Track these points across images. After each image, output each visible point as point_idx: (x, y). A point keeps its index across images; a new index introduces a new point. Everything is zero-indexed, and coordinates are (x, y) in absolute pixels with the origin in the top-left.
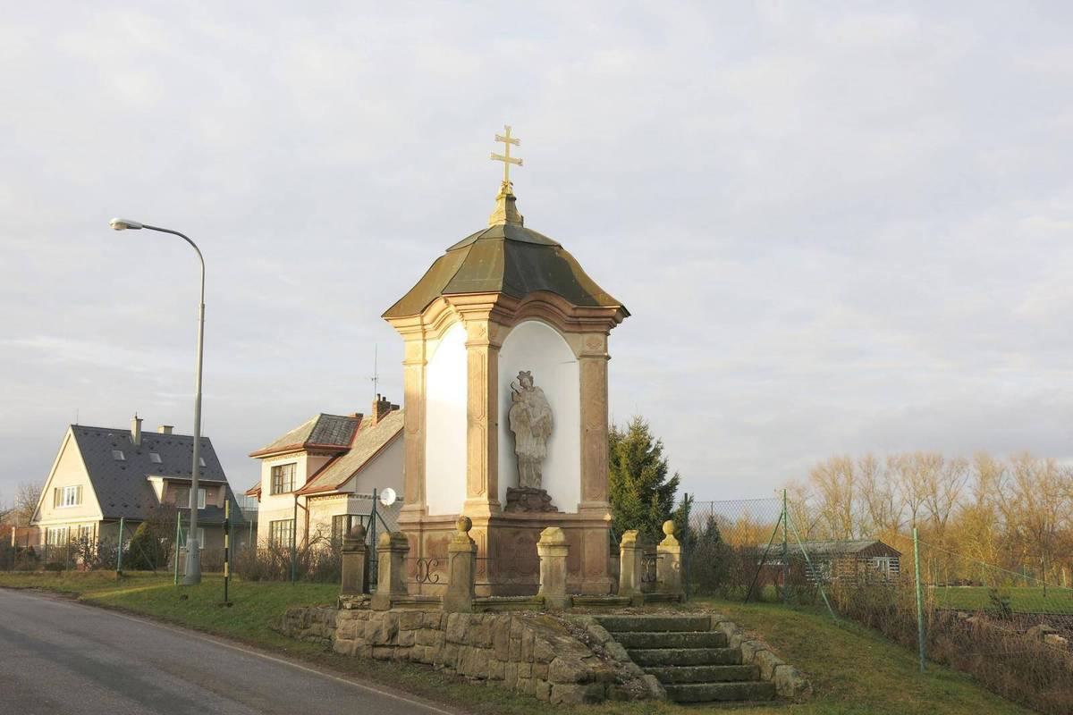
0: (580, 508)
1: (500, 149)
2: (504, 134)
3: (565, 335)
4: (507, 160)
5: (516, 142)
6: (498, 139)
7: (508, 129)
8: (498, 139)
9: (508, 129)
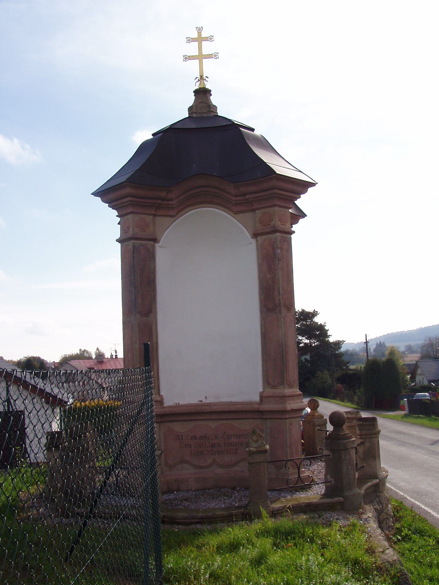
0: (262, 397)
1: (193, 49)
2: (195, 35)
3: (237, 216)
4: (201, 57)
5: (210, 39)
6: (190, 40)
7: (199, 30)
8: (190, 40)
9: (199, 30)
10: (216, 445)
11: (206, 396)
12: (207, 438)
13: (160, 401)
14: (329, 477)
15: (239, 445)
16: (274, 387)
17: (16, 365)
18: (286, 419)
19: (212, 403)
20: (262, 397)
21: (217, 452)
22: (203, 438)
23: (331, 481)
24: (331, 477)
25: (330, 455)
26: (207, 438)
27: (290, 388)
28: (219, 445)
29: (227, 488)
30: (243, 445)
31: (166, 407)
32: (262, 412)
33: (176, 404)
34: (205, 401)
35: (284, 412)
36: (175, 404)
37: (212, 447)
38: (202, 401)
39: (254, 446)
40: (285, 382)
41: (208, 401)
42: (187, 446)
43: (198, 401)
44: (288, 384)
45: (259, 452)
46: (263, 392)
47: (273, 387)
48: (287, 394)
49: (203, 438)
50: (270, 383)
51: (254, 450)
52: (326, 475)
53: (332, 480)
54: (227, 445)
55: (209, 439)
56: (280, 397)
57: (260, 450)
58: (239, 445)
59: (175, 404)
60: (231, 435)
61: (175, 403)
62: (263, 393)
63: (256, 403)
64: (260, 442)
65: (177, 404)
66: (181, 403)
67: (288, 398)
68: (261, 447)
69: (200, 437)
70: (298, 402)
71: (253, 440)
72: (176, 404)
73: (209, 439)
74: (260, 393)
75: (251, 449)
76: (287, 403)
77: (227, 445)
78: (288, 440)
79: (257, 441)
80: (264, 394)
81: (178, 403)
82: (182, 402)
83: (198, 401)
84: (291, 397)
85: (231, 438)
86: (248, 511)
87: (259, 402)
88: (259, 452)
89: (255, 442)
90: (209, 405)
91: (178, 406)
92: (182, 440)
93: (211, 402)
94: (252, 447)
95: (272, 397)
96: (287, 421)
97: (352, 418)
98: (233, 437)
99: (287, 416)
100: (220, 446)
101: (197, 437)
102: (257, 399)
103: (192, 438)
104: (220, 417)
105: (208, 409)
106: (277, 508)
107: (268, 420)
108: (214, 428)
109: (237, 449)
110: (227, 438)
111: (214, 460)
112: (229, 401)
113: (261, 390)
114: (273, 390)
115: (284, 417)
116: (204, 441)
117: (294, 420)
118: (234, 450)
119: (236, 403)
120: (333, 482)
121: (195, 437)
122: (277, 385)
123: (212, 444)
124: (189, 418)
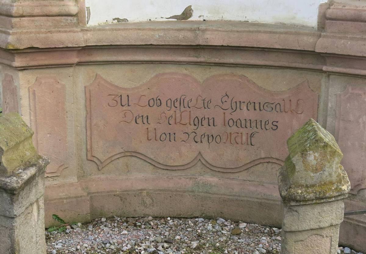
10: (205, 123)
12: (186, 105)
13: (75, 15)
15: (259, 126)
17: (325, 13)
21: (206, 137)
22: (177, 104)
26: (186, 105)
28: (211, 121)
30: (267, 127)
48: (75, 53)
54: (231, 123)
58: (259, 126)
73: (189, 107)
77: (231, 123)
80: (330, 12)
82: (134, 17)
98: (245, 108)
100: (214, 125)
103: (152, 102)
109: (252, 135)
110: (232, 109)
112: (145, 19)
118: (244, 138)
124: (153, 58)
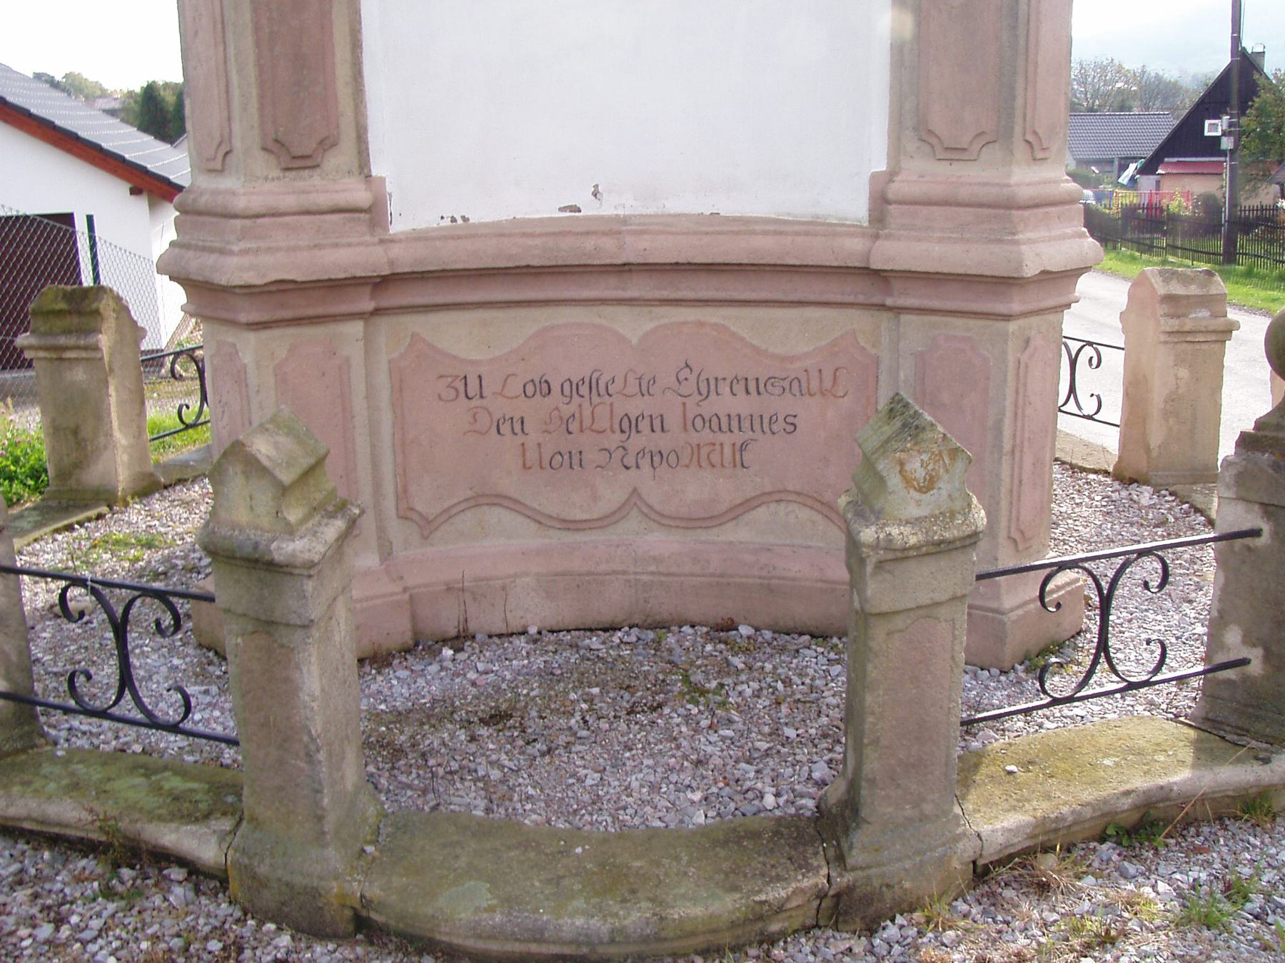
10: (644, 425)
11: (596, 186)
12: (603, 391)
14: (1233, 637)
16: (955, 153)
18: (1007, 317)
19: (624, 220)
20: (881, 203)
22: (584, 390)
23: (1244, 662)
24: (1248, 640)
25: (1255, 533)
27: (1034, 160)
29: (693, 626)
30: (775, 428)
31: (400, 241)
32: (880, 277)
33: (453, 220)
34: (590, 209)
35: (1006, 283)
36: (447, 222)
37: (622, 431)
38: (579, 211)
39: (914, 512)
40: (1018, 129)
41: (608, 208)
42: (505, 428)
43: (561, 209)
44: (1027, 142)
45: (940, 548)
46: (891, 175)
47: (948, 155)
48: (1025, 193)
49: (584, 390)
50: (930, 132)
51: (913, 540)
52: (1217, 625)
53: (1256, 655)
55: (610, 396)
56: (989, 206)
57: (947, 535)
58: (757, 426)
59: (447, 222)
60: (716, 379)
61: (448, 214)
62: (891, 181)
63: (852, 230)
64: (944, 487)
65: (460, 221)
66: (474, 219)
67: (1026, 213)
68: (953, 515)
69: (567, 386)
70: (1064, 237)
71: (908, 481)
72: (453, 220)
73: (610, 396)
74: (874, 177)
75: (895, 531)
76: (1020, 237)
77: (699, 422)
78: (1008, 421)
79: (929, 485)
81: (465, 219)
82: (481, 214)
83: (561, 209)
84: (1037, 206)
85: (718, 394)
86: (848, 878)
87: (866, 224)
88: (940, 548)
89: (920, 490)
90: (616, 227)
91: (461, 231)
92: (482, 397)
93: (621, 212)
94: (900, 522)
95: (945, 203)
96: (1012, 326)
97: (1188, 297)
98: (728, 389)
99: (1016, 307)
100: (663, 430)
101: (556, 387)
102: (856, 208)
104: (665, 294)
105: (610, 251)
106: (1001, 840)
107: (905, 318)
108: (635, 341)
109: (743, 447)
111: (635, 490)
113: (881, 166)
114: (943, 170)
115: (1001, 308)
116: (586, 405)
117: (1034, 320)
118: (727, 451)
119: (744, 226)
120: (1256, 667)
121: (545, 386)
122: (971, 143)
123: (626, 420)
124: (513, 507)
